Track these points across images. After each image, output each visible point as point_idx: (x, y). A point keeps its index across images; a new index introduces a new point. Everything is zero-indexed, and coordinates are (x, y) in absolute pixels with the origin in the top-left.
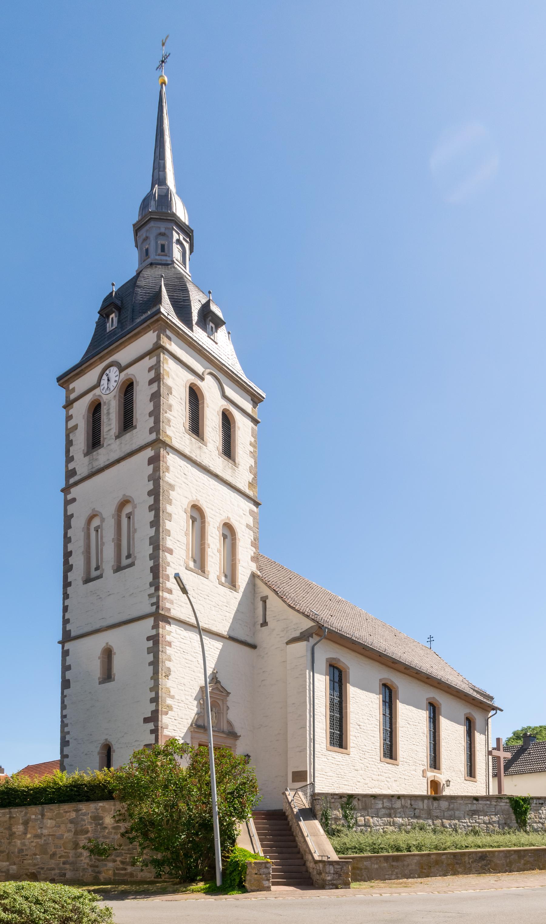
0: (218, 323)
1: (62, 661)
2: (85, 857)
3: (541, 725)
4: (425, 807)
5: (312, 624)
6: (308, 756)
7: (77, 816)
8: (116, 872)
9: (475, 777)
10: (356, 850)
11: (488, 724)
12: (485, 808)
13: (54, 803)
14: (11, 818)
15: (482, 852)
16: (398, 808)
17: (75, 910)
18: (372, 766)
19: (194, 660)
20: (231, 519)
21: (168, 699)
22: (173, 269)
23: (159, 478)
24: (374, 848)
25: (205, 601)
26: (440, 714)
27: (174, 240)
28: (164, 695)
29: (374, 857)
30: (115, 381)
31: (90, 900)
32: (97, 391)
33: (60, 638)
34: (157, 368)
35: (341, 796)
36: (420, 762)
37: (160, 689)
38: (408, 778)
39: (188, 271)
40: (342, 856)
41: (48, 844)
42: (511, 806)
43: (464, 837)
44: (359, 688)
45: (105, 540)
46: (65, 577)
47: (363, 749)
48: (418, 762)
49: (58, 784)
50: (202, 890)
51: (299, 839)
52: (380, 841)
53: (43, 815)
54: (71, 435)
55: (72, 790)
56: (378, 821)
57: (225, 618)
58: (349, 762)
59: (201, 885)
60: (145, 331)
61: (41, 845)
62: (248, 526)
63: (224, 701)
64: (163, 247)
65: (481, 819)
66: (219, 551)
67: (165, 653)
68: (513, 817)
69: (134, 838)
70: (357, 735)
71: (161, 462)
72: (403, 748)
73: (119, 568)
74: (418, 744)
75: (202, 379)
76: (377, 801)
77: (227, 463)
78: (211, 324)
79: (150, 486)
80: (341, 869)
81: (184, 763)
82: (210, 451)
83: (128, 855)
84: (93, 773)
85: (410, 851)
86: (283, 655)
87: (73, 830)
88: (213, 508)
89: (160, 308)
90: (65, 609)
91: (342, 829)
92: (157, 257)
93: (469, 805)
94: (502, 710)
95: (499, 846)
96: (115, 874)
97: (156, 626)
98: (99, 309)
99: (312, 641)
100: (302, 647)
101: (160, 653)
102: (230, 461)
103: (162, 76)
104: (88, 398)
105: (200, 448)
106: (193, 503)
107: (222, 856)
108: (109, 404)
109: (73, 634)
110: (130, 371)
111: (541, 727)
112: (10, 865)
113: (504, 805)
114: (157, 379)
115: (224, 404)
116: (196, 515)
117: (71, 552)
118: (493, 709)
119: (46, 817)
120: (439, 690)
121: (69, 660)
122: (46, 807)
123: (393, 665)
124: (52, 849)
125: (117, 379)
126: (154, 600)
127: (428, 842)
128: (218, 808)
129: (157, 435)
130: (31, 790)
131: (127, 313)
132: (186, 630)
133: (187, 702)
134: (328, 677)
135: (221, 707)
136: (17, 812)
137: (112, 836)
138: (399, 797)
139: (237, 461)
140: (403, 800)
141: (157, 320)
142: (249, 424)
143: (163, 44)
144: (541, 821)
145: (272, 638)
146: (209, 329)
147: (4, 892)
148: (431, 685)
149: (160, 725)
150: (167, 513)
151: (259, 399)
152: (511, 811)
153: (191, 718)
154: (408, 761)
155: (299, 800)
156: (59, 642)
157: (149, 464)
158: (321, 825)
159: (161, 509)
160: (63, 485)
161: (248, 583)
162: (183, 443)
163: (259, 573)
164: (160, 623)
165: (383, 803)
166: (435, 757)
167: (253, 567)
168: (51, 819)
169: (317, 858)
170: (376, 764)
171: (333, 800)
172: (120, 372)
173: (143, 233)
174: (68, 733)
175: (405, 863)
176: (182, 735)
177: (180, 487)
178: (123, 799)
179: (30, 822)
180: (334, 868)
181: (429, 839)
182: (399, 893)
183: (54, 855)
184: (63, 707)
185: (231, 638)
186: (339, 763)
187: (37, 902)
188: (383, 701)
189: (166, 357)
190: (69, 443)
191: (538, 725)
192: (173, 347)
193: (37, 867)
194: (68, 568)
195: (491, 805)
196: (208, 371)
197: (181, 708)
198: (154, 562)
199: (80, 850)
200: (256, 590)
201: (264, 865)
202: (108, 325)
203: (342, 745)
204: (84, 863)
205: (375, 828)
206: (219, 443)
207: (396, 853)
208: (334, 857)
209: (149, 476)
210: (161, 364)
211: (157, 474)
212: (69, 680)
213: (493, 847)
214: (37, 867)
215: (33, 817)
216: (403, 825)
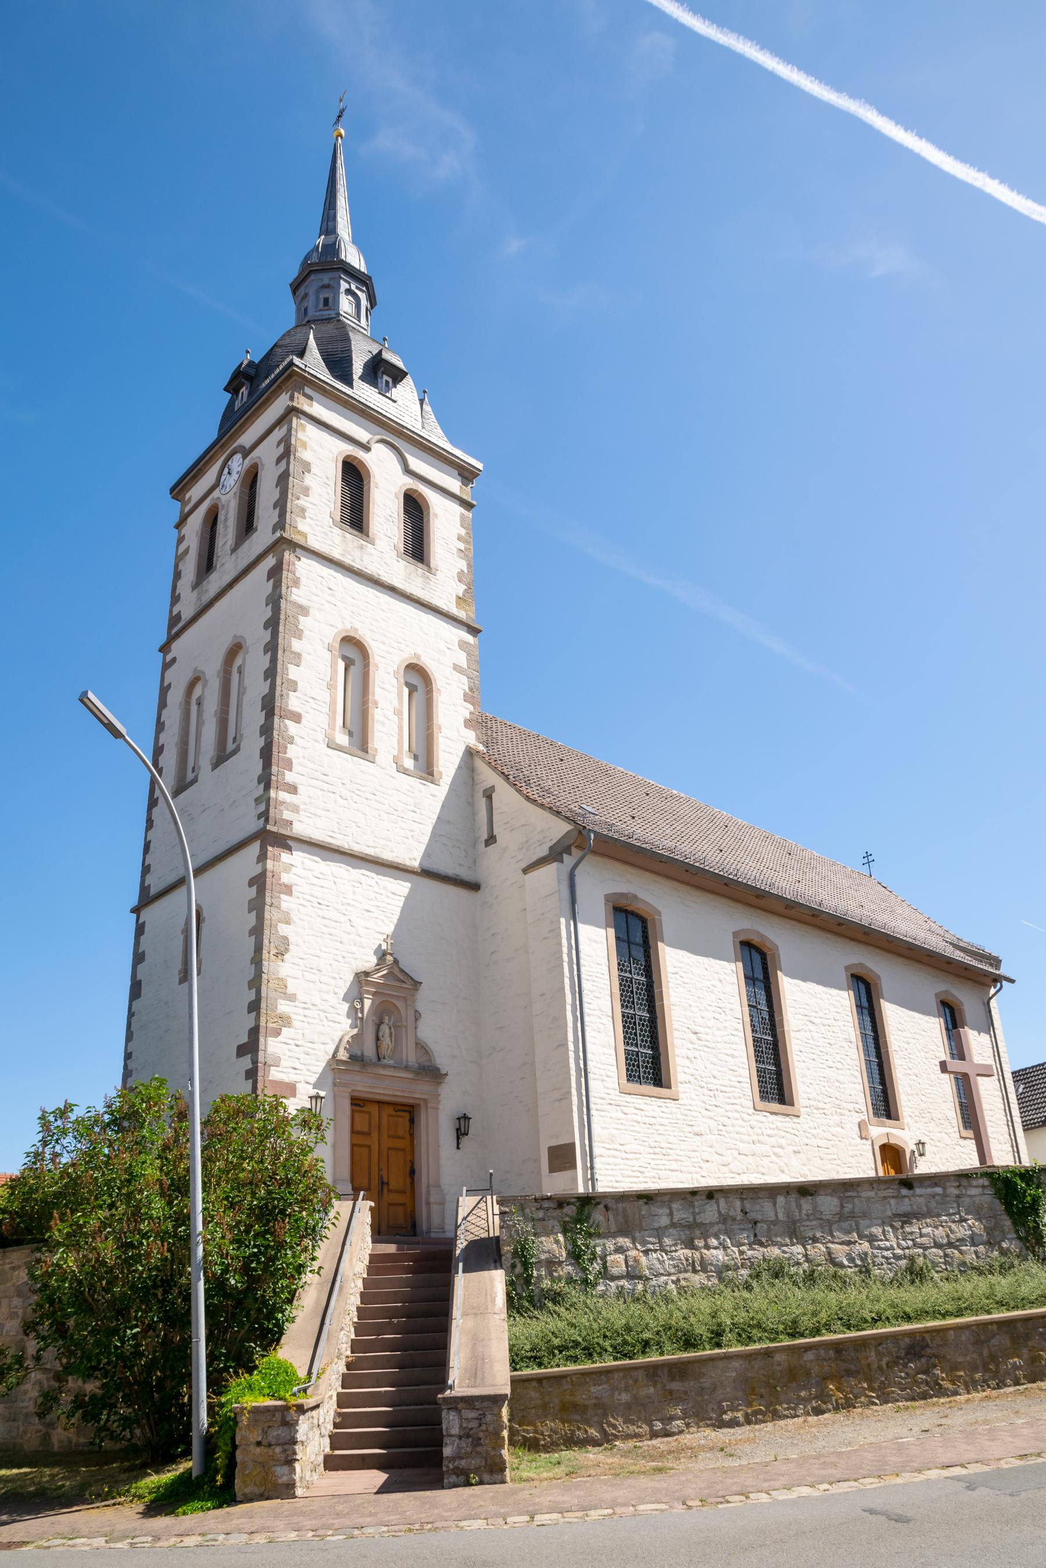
0: (398, 375)
5: (567, 827)
6: (575, 1108)
10: (578, 1351)
11: (990, 1011)
12: (933, 1204)
15: (911, 1334)
16: (711, 1224)
18: (736, 1122)
19: (342, 918)
20: (423, 658)
21: (281, 1001)
24: (625, 1343)
28: (272, 994)
29: (617, 1369)
32: (216, 494)
36: (851, 1106)
42: (998, 1194)
44: (715, 957)
47: (711, 1086)
48: (845, 1105)
56: (662, 1262)
57: (409, 834)
58: (679, 1116)
60: (276, 394)
62: (456, 668)
64: (326, 301)
65: (927, 1235)
66: (398, 713)
67: (279, 907)
68: (1008, 1223)
70: (691, 1054)
71: (285, 573)
72: (804, 1076)
74: (839, 1065)
75: (367, 448)
76: (654, 1209)
78: (385, 378)
80: (480, 1419)
85: (719, 1345)
86: (524, 891)
92: (318, 313)
93: (893, 1201)
94: (1012, 981)
95: (959, 1313)
97: (262, 857)
99: (569, 860)
100: (550, 875)
101: (267, 908)
106: (344, 634)
108: (228, 506)
109: (153, 891)
113: (979, 1193)
114: (287, 453)
115: (410, 483)
116: (353, 653)
120: (871, 948)
123: (757, 902)
127: (772, 1317)
132: (324, 860)
138: (711, 1194)
139: (432, 565)
140: (722, 1202)
142: (457, 509)
149: (261, 1059)
151: (472, 473)
152: (1000, 1207)
153: (333, 1040)
154: (821, 1105)
156: (132, 911)
161: (459, 767)
163: (481, 748)
167: (470, 738)
170: (745, 1116)
171: (541, 1214)
173: (301, 291)
175: (706, 1382)
176: (313, 1079)
180: (461, 1419)
188: (746, 977)
190: (177, 575)
192: (317, 409)
195: (945, 1195)
196: (379, 437)
197: (310, 1020)
201: (278, 1415)
203: (660, 1080)
205: (654, 1283)
206: (399, 539)
213: (944, 1315)
216: (728, 1268)
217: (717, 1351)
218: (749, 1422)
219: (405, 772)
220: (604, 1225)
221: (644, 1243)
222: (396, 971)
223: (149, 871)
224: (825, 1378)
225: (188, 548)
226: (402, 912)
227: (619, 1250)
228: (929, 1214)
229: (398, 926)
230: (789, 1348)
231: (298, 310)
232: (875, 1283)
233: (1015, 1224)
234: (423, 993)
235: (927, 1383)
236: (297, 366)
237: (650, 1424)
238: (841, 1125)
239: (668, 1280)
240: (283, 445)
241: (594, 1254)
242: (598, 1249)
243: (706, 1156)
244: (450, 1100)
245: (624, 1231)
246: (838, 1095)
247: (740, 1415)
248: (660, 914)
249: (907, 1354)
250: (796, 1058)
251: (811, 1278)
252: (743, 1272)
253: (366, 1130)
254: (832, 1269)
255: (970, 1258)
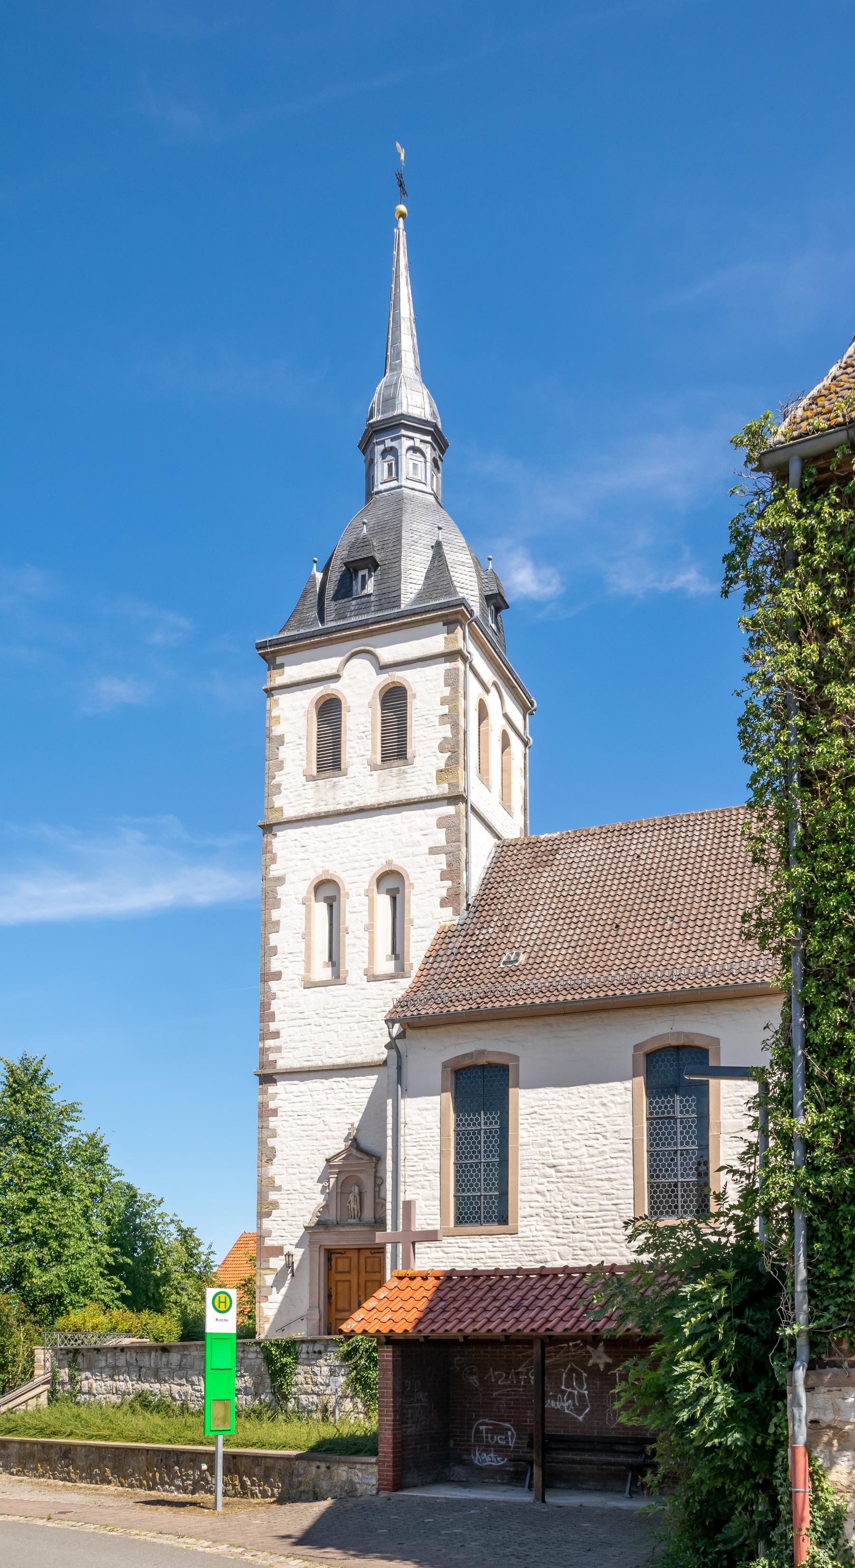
19: (317, 1121)
75: (336, 677)
132: (301, 1081)
133: (304, 1190)
144: (316, 1389)
226: (369, 1102)
245: (89, 1369)
253: (347, 1269)
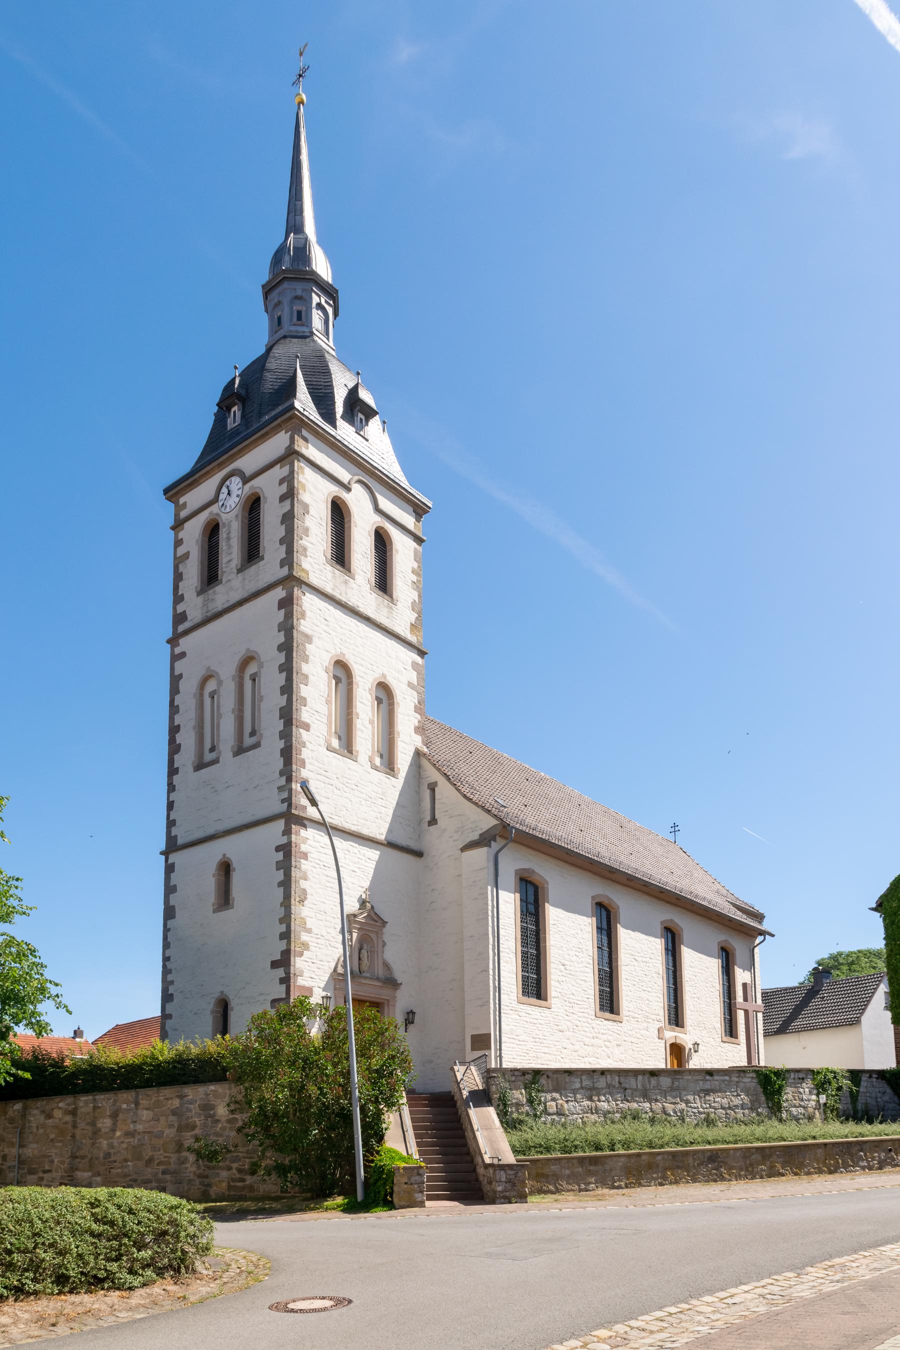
0: (369, 413)
1: (165, 879)
2: (191, 1165)
3: (859, 948)
4: (639, 1086)
5: (494, 822)
6: (492, 1012)
7: (181, 1105)
8: (232, 1184)
9: (737, 1038)
10: (542, 1149)
11: (753, 956)
12: (723, 1085)
13: (152, 1086)
14: (95, 1108)
15: (711, 1150)
16: (602, 1089)
17: (173, 1222)
20: (388, 677)
21: (303, 933)
22: (312, 344)
23: (292, 627)
24: (565, 1146)
25: (351, 791)
26: (681, 943)
27: (314, 305)
28: (298, 929)
30: (238, 496)
31: (189, 1211)
32: (214, 509)
33: (163, 847)
34: (289, 480)
35: (524, 1072)
36: (654, 1017)
37: (293, 920)
38: (635, 1042)
39: (331, 344)
40: (523, 1157)
41: (143, 1145)
43: (692, 1130)
45: (222, 711)
46: (171, 762)
48: (651, 1016)
49: (157, 1059)
50: (338, 1206)
51: (468, 1134)
52: (574, 1136)
53: (137, 1104)
54: (180, 566)
55: (174, 1067)
56: (575, 1107)
59: (340, 1200)
61: (134, 1147)
62: (410, 685)
63: (379, 934)
64: (299, 313)
65: (718, 1102)
66: (371, 722)
67: (300, 869)
68: (763, 1098)
69: (253, 1135)
70: (560, 979)
72: (628, 996)
73: (240, 750)
74: (650, 989)
75: (348, 489)
76: (573, 1079)
77: (384, 601)
78: (360, 415)
79: (281, 638)
80: (515, 1175)
81: (315, 1030)
82: (359, 587)
83: (247, 1160)
84: (203, 1042)
85: (614, 1150)
86: (457, 865)
87: (176, 1124)
88: (363, 662)
89: (293, 403)
90: (170, 806)
91: (526, 1119)
92: (293, 328)
93: (701, 1082)
94: (773, 936)
95: (736, 1142)
96: (230, 1187)
97: (287, 832)
98: (217, 401)
99: (495, 846)
100: (481, 855)
102: (386, 597)
103: (299, 94)
104: (203, 517)
105: (346, 582)
107: (364, 1160)
108: (229, 526)
109: (180, 841)
110: (255, 483)
111: (859, 951)
112: (93, 1176)
113: (750, 1081)
114: (290, 495)
115: (378, 520)
116: (341, 674)
117: (179, 726)
118: (761, 934)
119: (141, 1106)
121: (175, 878)
122: (142, 1091)
124: (147, 1153)
125: (240, 492)
126: (285, 795)
127: (639, 1137)
128: (359, 1092)
129: (289, 570)
130: (122, 1067)
131: (254, 407)
134: (518, 895)
135: (375, 942)
136: (104, 1099)
137: (226, 1133)
138: (603, 1072)
139: (394, 597)
140: (609, 1077)
141: (291, 418)
142: (412, 544)
143: (301, 54)
144: (802, 1103)
145: (443, 842)
146: (358, 423)
147: (96, 1199)
148: (668, 902)
149: (292, 971)
150: (303, 674)
151: (423, 510)
154: (636, 1015)
155: (470, 1079)
156: (162, 853)
157: (279, 609)
158: (498, 1114)
159: (294, 669)
160: (169, 634)
161: (411, 765)
162: (323, 578)
163: (425, 750)
164: (293, 826)
165: (581, 1082)
166: (676, 1008)
168: (147, 1109)
169: (488, 1161)
170: (590, 1021)
171: (513, 1079)
172: (244, 484)
173: (274, 296)
174: (172, 982)
175: (607, 1167)
176: (322, 985)
177: (319, 638)
178: (239, 1080)
179: (121, 1115)
181: (644, 1131)
182: (584, 1208)
183: (150, 1160)
184: (166, 945)
185: (390, 845)
186: (535, 1021)
187: (131, 1212)
189: (302, 464)
190: (178, 577)
191: (854, 948)
192: (311, 451)
193: (128, 1178)
194: (174, 748)
196: (356, 478)
198: (285, 743)
199: (185, 1154)
200: (422, 773)
201: (415, 1171)
202: (230, 421)
204: (190, 1172)
207: (594, 1153)
208: (510, 1158)
209: (279, 625)
210: (296, 476)
211: (290, 621)
212: (174, 907)
213: (728, 1143)
214: (128, 1178)
215: (125, 1106)
216: (609, 1112)
217: (612, 1152)
218: (627, 1187)
219: (375, 768)
220: (546, 1086)
221: (566, 1096)
222: (372, 914)
223: (175, 825)
224: (666, 1169)
225: (188, 553)
227: (554, 1100)
228: (720, 1091)
229: (372, 882)
230: (650, 1153)
231: (271, 319)
232: (686, 1123)
233: (767, 1099)
234: (387, 930)
235: (717, 1175)
236: (298, 410)
237: (579, 1186)
238: (647, 1029)
239: (579, 1119)
240: (286, 484)
241: (540, 1101)
242: (543, 1099)
243: (565, 1045)
244: (402, 1001)
245: (556, 1090)
246: (647, 1009)
247: (623, 1184)
248: (547, 883)
249: (708, 1160)
250: (623, 983)
251: (652, 1121)
252: (617, 1115)
254: (664, 1116)
255: (740, 1116)
